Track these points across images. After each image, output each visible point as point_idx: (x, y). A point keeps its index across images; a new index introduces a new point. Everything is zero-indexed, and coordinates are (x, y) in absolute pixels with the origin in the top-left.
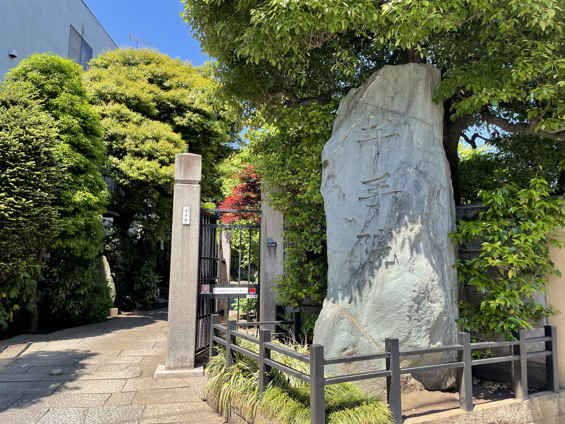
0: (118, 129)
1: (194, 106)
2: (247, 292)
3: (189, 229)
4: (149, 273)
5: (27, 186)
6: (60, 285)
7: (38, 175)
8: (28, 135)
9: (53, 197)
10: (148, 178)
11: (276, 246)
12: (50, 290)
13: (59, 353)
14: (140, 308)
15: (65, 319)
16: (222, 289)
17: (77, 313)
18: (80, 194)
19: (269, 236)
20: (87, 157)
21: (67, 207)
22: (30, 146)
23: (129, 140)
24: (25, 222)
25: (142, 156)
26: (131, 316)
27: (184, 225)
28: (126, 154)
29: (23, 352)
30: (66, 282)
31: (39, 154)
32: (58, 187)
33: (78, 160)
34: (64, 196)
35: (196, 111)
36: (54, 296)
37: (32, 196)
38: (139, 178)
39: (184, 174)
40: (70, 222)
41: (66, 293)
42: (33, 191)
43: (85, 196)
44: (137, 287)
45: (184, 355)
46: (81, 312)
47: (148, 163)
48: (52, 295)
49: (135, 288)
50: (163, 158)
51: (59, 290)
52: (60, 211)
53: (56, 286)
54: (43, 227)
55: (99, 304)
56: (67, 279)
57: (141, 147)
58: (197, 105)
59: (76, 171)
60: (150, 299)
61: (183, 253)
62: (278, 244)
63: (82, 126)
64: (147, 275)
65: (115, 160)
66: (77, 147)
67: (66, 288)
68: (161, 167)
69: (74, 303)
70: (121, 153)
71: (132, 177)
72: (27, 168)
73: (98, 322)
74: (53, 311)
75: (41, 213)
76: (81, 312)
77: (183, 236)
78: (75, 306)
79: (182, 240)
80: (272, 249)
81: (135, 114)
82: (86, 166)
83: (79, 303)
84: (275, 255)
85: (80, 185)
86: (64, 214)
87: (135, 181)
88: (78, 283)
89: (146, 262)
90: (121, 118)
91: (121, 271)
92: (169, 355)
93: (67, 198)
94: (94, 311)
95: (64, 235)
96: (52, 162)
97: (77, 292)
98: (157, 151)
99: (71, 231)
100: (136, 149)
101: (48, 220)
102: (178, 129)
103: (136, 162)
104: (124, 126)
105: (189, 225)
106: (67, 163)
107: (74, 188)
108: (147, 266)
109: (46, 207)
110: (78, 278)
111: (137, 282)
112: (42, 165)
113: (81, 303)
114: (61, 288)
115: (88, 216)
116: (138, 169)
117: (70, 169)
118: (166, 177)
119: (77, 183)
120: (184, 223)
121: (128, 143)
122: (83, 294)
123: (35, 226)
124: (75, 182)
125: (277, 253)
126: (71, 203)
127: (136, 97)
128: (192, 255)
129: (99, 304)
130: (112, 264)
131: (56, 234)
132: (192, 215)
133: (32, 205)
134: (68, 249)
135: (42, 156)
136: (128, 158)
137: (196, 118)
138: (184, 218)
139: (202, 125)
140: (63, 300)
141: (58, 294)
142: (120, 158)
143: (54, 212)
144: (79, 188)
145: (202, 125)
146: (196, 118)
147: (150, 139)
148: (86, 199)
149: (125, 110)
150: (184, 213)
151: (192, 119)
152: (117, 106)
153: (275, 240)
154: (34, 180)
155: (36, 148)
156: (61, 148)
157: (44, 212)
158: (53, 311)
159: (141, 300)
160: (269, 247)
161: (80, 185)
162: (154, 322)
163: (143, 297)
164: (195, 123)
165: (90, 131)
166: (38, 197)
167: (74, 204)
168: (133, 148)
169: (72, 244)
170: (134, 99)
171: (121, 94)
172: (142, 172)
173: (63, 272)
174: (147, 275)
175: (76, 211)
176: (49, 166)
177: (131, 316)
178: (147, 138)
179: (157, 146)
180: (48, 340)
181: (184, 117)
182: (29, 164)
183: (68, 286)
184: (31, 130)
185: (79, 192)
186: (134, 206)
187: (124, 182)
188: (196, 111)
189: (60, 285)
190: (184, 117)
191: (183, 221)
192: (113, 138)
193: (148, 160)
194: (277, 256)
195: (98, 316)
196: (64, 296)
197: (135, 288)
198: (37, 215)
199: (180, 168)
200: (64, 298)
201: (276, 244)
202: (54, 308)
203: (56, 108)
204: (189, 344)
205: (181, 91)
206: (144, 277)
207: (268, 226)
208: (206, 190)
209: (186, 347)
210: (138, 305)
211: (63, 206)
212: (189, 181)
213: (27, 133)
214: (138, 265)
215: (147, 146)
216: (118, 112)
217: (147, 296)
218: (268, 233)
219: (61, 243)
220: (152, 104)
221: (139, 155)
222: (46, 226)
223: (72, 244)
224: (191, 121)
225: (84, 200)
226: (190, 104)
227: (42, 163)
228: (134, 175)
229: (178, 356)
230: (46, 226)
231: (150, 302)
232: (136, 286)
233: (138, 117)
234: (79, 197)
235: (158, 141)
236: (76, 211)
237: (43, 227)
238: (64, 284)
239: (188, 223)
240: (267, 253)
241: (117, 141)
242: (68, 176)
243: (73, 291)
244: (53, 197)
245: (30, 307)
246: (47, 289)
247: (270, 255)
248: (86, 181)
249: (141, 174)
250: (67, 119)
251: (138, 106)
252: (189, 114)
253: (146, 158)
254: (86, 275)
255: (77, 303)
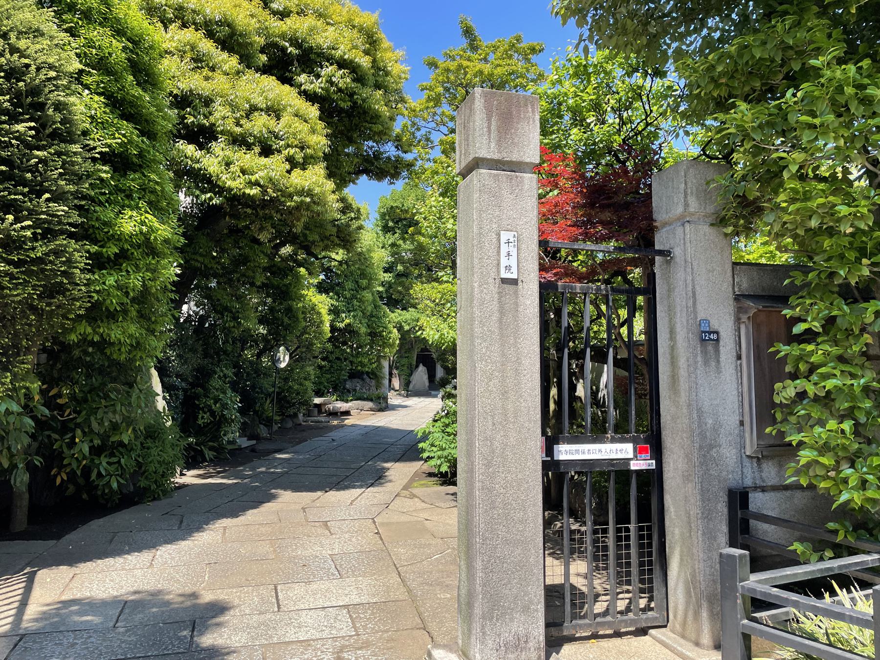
0: (194, 82)
1: (338, 54)
2: (631, 456)
3: (516, 293)
4: (225, 393)
5: (15, 186)
6: (78, 425)
7: (41, 161)
8: (16, 56)
9: (75, 218)
10: (264, 192)
11: (718, 340)
12: (57, 436)
13: (124, 607)
14: (211, 460)
15: (85, 496)
16: (574, 447)
17: (115, 485)
18: (131, 217)
19: (701, 315)
20: (142, 133)
21: (102, 246)
22: (21, 84)
23: (220, 108)
24: (12, 277)
25: (249, 147)
26: (210, 481)
27: (504, 281)
28: (216, 139)
29: (24, 603)
30: (92, 419)
31: (42, 106)
32: (84, 197)
33: (124, 135)
34: (98, 219)
35: (342, 64)
36: (65, 450)
37: (28, 210)
38: (248, 191)
39: (499, 142)
40: (111, 281)
41: (91, 441)
42: (31, 200)
43: (143, 223)
44: (203, 419)
45: (521, 631)
46: (122, 481)
47: (264, 160)
48: (61, 447)
49: (200, 422)
50: (292, 151)
51: (74, 437)
52: (92, 256)
53: (65, 428)
54: (52, 291)
55: (159, 462)
56: (94, 411)
57: (247, 125)
58: (343, 51)
59: (120, 161)
60: (229, 442)
61: (503, 355)
62: (722, 334)
63: (129, 60)
64: (221, 396)
65: (190, 149)
66: (121, 107)
67: (91, 431)
68: (289, 172)
69: (108, 463)
70: (203, 136)
71: (230, 189)
72: (16, 138)
73: (154, 499)
74: (58, 481)
75: (47, 254)
76: (122, 481)
77: (502, 311)
78: (111, 469)
79: (500, 321)
80: (710, 348)
81: (225, 55)
82: (141, 155)
83: (119, 462)
84: (718, 362)
85: (129, 197)
86: (98, 263)
87: (236, 200)
88: (118, 418)
89: (218, 370)
90: (199, 61)
91: (178, 389)
92: (484, 633)
93: (105, 224)
94: (146, 478)
95: (97, 313)
96: (70, 133)
97: (115, 438)
98: (276, 137)
99: (113, 302)
100: (238, 130)
101: (64, 273)
102: (310, 97)
103: (238, 155)
104: (207, 78)
105: (514, 282)
106: (102, 141)
107: (116, 203)
108: (220, 377)
109: (61, 241)
110: (118, 408)
111: (202, 409)
112: (48, 136)
113: (122, 461)
114: (79, 432)
115: (147, 270)
116: (244, 172)
117: (105, 158)
118: (301, 192)
119: (124, 191)
120: (504, 275)
121: (220, 114)
122: (126, 442)
123: (34, 287)
124: (118, 190)
125: (723, 358)
126: (113, 236)
127: (226, 19)
128: (526, 362)
129: (159, 462)
130: (163, 372)
131: (80, 308)
132: (522, 255)
133: (29, 233)
134: (104, 344)
135: (50, 112)
136: (219, 147)
137: (342, 78)
138: (504, 262)
139: (351, 95)
140: (84, 458)
141: (72, 444)
142: (201, 147)
143: (78, 252)
144: (126, 202)
145: (351, 95)
146: (342, 78)
147: (262, 110)
148: (144, 229)
149: (207, 46)
150: (504, 249)
151: (334, 79)
152: (189, 35)
153: (715, 325)
154: (33, 170)
155: (35, 91)
156: (84, 105)
157: (57, 253)
158: (58, 481)
159: (211, 444)
160: (703, 340)
161: (129, 197)
162: (271, 498)
163: (216, 437)
164: (340, 90)
165: (146, 76)
166: (43, 213)
167: (119, 240)
168: (230, 125)
169: (115, 333)
170: (220, 23)
171: (194, 11)
172: (253, 178)
173: (80, 395)
174: (221, 396)
175: (123, 256)
176: (64, 141)
177: (210, 481)
178: (254, 109)
179: (279, 127)
180: (71, 559)
181: (318, 76)
182: (20, 127)
183: (95, 426)
184: (22, 44)
185: (128, 212)
186: (200, 259)
187: (211, 199)
188: (342, 64)
189: (78, 425)
190: (318, 76)
191: (503, 270)
192: (182, 101)
193: (260, 154)
194: (722, 364)
195: (154, 487)
196: (86, 449)
197: (200, 422)
198: (39, 261)
199: (489, 128)
200: (87, 454)
201: (717, 333)
202: (59, 473)
203: (70, 10)
204: (531, 602)
205: (309, 22)
206: (217, 400)
207: (698, 288)
208: (328, 234)
209: (526, 609)
210: (209, 454)
211: (94, 241)
212: (511, 162)
213: (14, 50)
214: (202, 376)
215: (259, 124)
216: (193, 48)
217: (225, 435)
218: (699, 307)
219: (89, 330)
220: (257, 39)
221: (240, 141)
222: (60, 289)
223: (115, 333)
224: (332, 83)
225: (141, 233)
226: (329, 48)
227: (49, 131)
228: (236, 184)
229: (507, 636)
230: (60, 289)
231: (230, 447)
232: (203, 418)
233: (232, 62)
234: (129, 223)
235: (278, 118)
236: (123, 256)
237: (52, 291)
238: (87, 421)
239: (514, 276)
240: (699, 359)
241: (195, 108)
242: (105, 172)
243: (105, 437)
244: (75, 218)
245: (18, 480)
246: (47, 433)
247: (706, 363)
248: (143, 189)
249: (251, 184)
250: (100, 36)
251: (229, 39)
252: (328, 70)
253: (257, 149)
254: (133, 399)
255: (114, 463)
